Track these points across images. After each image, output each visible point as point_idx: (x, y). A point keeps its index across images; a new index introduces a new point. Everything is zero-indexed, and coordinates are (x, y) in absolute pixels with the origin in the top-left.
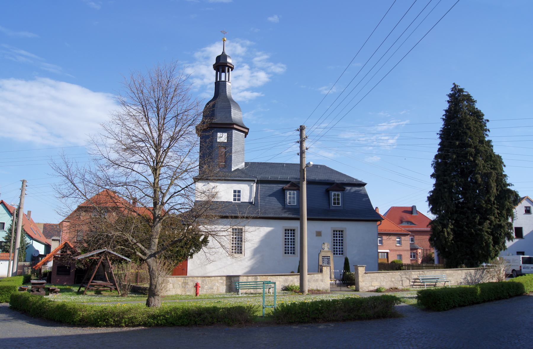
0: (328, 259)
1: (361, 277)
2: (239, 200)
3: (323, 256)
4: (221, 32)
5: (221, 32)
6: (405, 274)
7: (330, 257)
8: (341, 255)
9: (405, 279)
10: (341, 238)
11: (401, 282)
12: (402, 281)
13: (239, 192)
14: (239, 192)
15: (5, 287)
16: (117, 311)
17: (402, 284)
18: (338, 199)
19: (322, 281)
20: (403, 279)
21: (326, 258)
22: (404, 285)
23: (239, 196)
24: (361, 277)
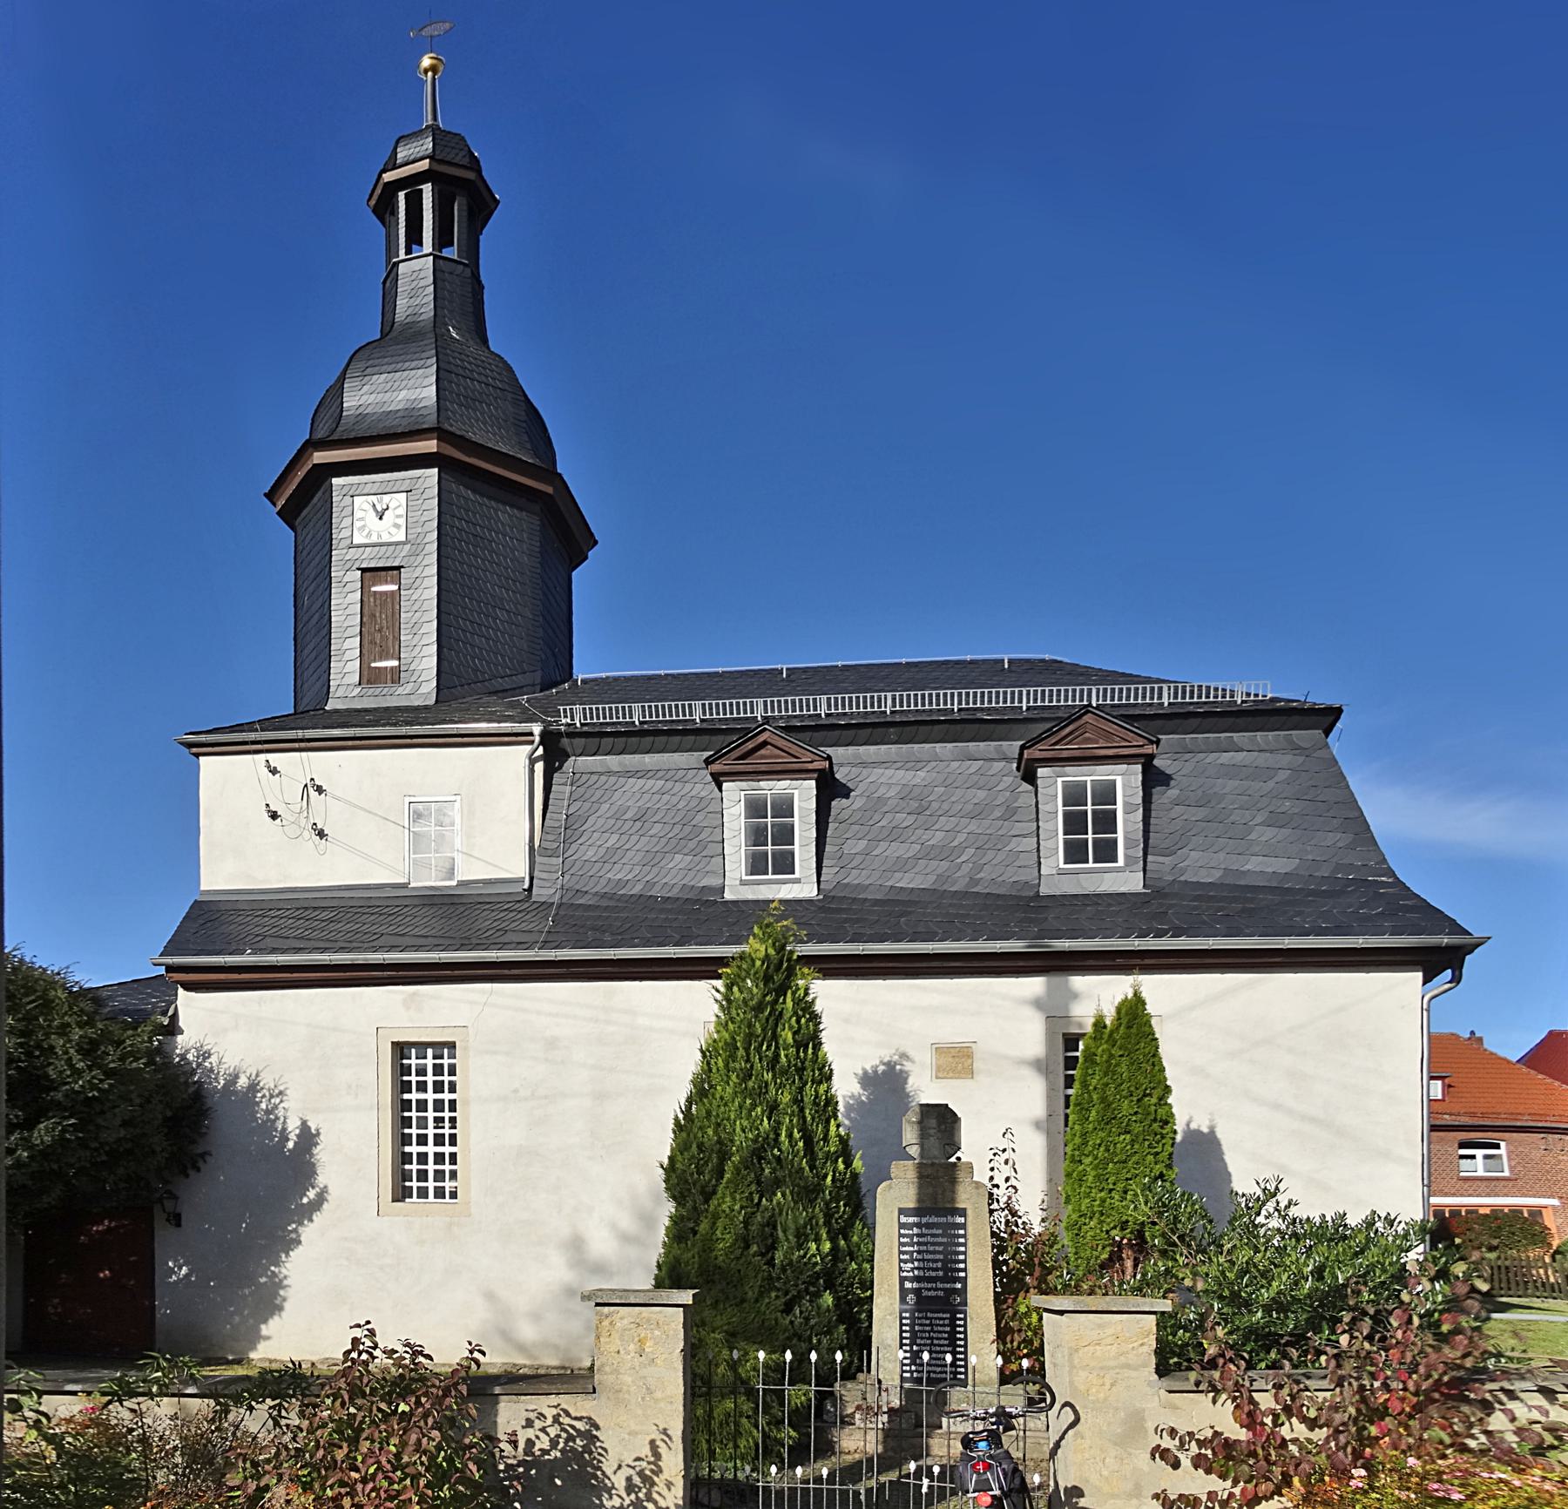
10: (446, 1096)
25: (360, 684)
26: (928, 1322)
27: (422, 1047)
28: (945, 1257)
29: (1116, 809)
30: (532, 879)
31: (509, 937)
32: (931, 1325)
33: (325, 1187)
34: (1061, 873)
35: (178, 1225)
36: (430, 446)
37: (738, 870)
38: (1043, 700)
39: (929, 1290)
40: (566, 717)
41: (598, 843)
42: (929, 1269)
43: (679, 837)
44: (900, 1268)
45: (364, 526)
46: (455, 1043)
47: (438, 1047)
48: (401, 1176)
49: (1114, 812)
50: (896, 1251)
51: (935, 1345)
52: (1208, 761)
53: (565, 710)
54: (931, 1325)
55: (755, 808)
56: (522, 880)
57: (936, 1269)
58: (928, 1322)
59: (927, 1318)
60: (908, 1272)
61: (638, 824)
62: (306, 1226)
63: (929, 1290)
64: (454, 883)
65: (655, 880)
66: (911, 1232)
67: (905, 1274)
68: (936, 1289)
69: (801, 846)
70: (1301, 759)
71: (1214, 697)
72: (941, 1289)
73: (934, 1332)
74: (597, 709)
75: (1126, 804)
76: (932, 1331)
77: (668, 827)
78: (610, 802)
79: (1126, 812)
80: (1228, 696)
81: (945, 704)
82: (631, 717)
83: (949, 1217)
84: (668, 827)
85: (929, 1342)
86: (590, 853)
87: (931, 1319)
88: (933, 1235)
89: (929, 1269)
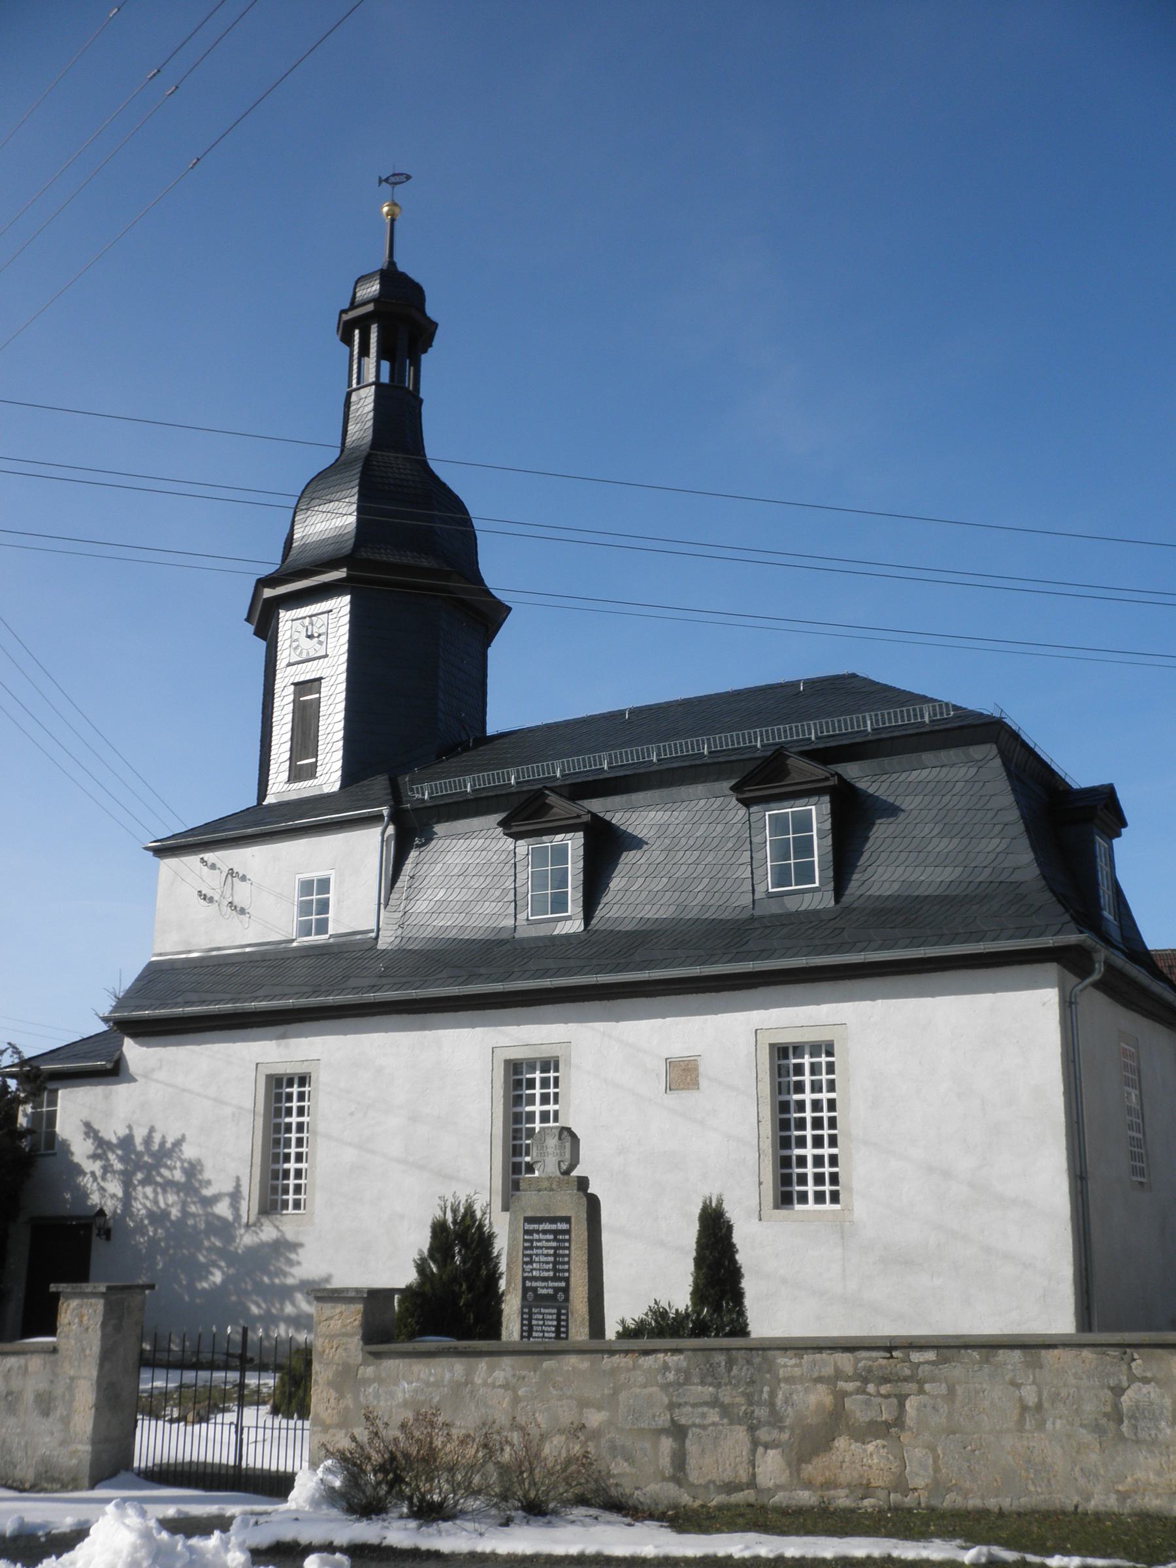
0: (556, 1233)
1: (330, 1384)
2: (322, 927)
3: (530, 1214)
4: (408, 177)
5: (408, 177)
6: (710, 1376)
7: (567, 1220)
8: (828, 1206)
9: (713, 1416)
10: (824, 1096)
11: (667, 1444)
12: (679, 1432)
13: (324, 884)
14: (324, 884)
15: (373, 1344)
16: (14, 1481)
17: (680, 1461)
18: (804, 847)
19: (45, 1404)
20: (685, 1417)
21: (547, 1226)
22: (694, 1477)
23: (324, 906)
24: (330, 1384)
25: (288, 781)
26: (541, 1317)
27: (798, 1050)
28: (555, 1259)
29: (328, 899)
30: (378, 930)
31: (261, 993)
32: (543, 1319)
33: (440, 1198)
34: (771, 896)
35: (108, 1238)
36: (341, 574)
37: (764, 883)
38: (890, 721)
39: (543, 1288)
40: (418, 793)
41: (430, 898)
42: (543, 1270)
43: (489, 887)
44: (523, 1269)
45: (298, 646)
46: (508, 1063)
47: (816, 1049)
48: (786, 1180)
49: (812, 835)
50: (521, 1254)
51: (546, 1338)
52: (900, 779)
53: (417, 788)
54: (543, 1319)
55: (779, 824)
56: (372, 931)
57: (548, 1270)
58: (541, 1317)
59: (540, 1313)
60: (529, 1272)
61: (462, 878)
62: (101, 1238)
63: (543, 1288)
64: (326, 936)
65: (467, 925)
66: (531, 1237)
67: (526, 1275)
68: (548, 1288)
69: (573, 888)
70: (973, 771)
71: (732, 745)
72: (551, 1287)
73: (546, 1326)
74: (538, 767)
75: (818, 830)
76: (544, 1324)
77: (482, 879)
78: (443, 862)
79: (819, 838)
80: (945, 714)
81: (859, 726)
82: (601, 764)
83: (559, 1224)
84: (482, 879)
85: (541, 1334)
86: (423, 907)
87: (543, 1314)
88: (548, 1241)
89: (543, 1270)
